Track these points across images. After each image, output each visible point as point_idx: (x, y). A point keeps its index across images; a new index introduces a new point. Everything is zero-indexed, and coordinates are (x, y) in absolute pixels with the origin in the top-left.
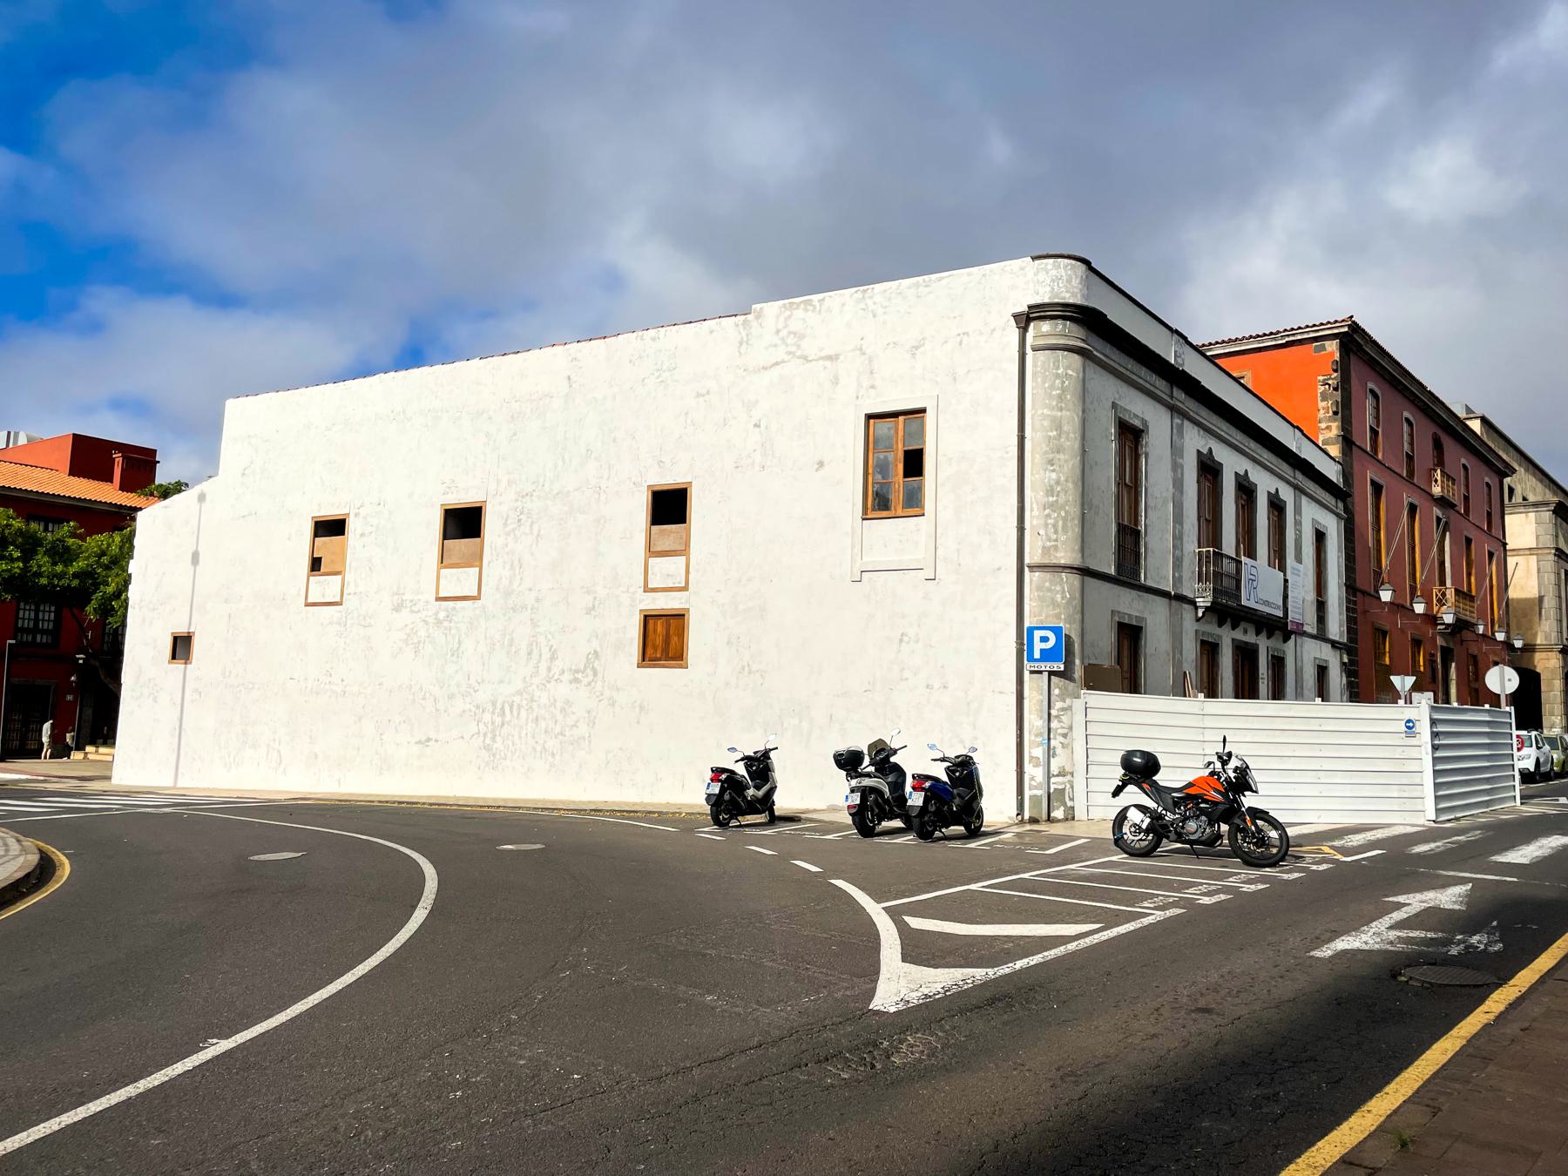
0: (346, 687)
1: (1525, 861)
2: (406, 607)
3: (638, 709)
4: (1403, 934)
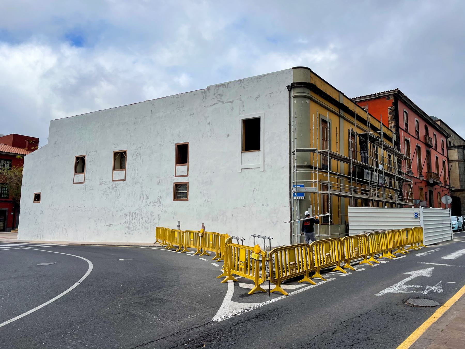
0: (85, 209)
1: (453, 258)
2: (103, 184)
3: (173, 214)
4: (408, 286)
